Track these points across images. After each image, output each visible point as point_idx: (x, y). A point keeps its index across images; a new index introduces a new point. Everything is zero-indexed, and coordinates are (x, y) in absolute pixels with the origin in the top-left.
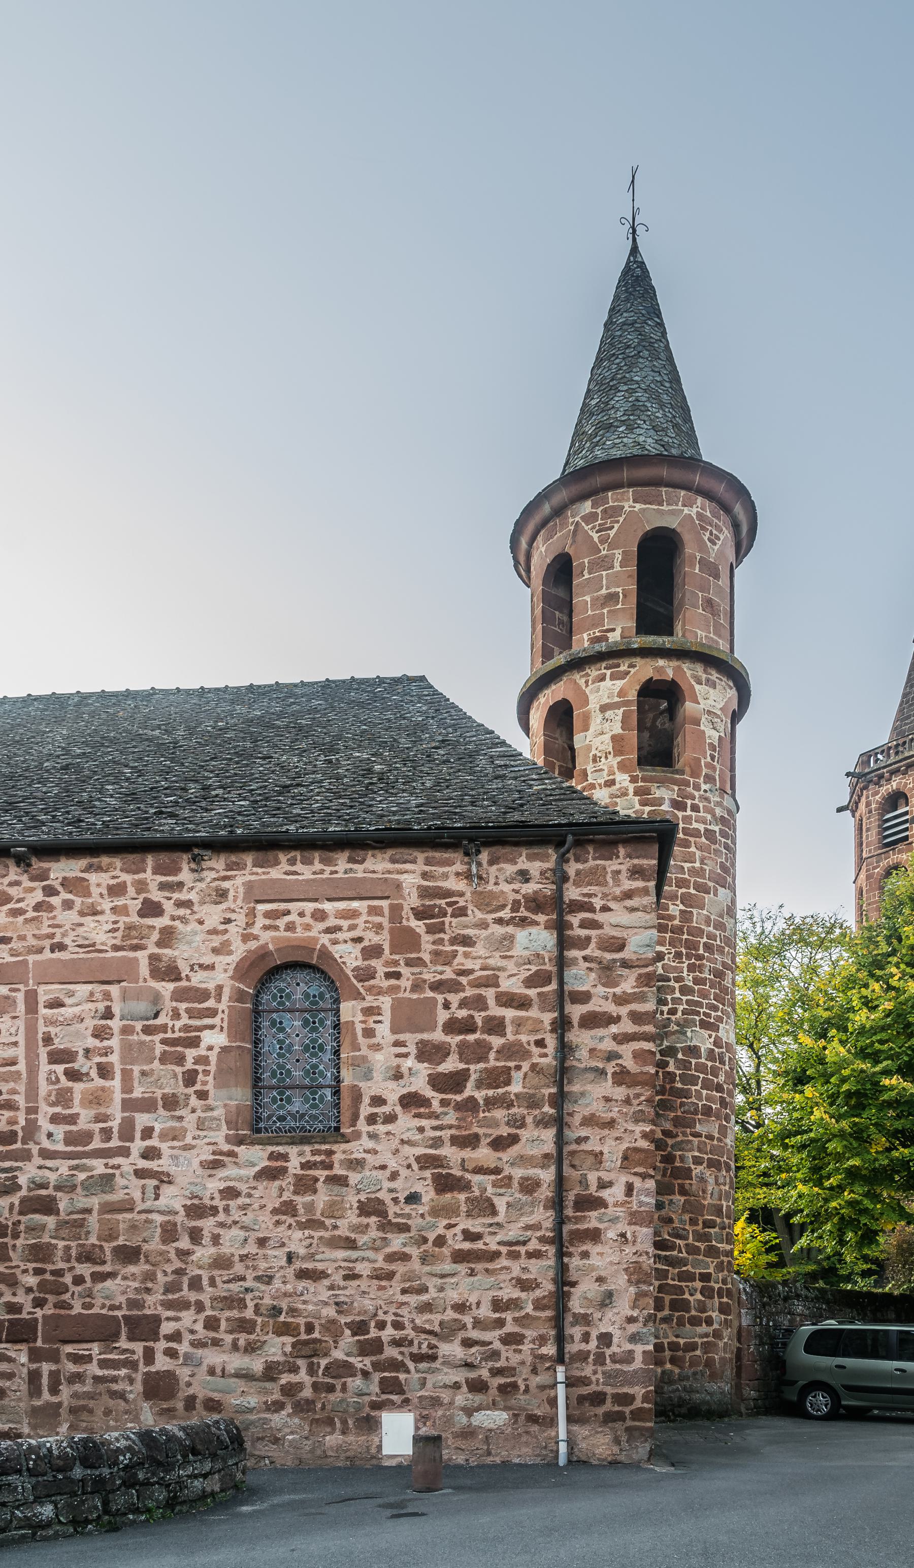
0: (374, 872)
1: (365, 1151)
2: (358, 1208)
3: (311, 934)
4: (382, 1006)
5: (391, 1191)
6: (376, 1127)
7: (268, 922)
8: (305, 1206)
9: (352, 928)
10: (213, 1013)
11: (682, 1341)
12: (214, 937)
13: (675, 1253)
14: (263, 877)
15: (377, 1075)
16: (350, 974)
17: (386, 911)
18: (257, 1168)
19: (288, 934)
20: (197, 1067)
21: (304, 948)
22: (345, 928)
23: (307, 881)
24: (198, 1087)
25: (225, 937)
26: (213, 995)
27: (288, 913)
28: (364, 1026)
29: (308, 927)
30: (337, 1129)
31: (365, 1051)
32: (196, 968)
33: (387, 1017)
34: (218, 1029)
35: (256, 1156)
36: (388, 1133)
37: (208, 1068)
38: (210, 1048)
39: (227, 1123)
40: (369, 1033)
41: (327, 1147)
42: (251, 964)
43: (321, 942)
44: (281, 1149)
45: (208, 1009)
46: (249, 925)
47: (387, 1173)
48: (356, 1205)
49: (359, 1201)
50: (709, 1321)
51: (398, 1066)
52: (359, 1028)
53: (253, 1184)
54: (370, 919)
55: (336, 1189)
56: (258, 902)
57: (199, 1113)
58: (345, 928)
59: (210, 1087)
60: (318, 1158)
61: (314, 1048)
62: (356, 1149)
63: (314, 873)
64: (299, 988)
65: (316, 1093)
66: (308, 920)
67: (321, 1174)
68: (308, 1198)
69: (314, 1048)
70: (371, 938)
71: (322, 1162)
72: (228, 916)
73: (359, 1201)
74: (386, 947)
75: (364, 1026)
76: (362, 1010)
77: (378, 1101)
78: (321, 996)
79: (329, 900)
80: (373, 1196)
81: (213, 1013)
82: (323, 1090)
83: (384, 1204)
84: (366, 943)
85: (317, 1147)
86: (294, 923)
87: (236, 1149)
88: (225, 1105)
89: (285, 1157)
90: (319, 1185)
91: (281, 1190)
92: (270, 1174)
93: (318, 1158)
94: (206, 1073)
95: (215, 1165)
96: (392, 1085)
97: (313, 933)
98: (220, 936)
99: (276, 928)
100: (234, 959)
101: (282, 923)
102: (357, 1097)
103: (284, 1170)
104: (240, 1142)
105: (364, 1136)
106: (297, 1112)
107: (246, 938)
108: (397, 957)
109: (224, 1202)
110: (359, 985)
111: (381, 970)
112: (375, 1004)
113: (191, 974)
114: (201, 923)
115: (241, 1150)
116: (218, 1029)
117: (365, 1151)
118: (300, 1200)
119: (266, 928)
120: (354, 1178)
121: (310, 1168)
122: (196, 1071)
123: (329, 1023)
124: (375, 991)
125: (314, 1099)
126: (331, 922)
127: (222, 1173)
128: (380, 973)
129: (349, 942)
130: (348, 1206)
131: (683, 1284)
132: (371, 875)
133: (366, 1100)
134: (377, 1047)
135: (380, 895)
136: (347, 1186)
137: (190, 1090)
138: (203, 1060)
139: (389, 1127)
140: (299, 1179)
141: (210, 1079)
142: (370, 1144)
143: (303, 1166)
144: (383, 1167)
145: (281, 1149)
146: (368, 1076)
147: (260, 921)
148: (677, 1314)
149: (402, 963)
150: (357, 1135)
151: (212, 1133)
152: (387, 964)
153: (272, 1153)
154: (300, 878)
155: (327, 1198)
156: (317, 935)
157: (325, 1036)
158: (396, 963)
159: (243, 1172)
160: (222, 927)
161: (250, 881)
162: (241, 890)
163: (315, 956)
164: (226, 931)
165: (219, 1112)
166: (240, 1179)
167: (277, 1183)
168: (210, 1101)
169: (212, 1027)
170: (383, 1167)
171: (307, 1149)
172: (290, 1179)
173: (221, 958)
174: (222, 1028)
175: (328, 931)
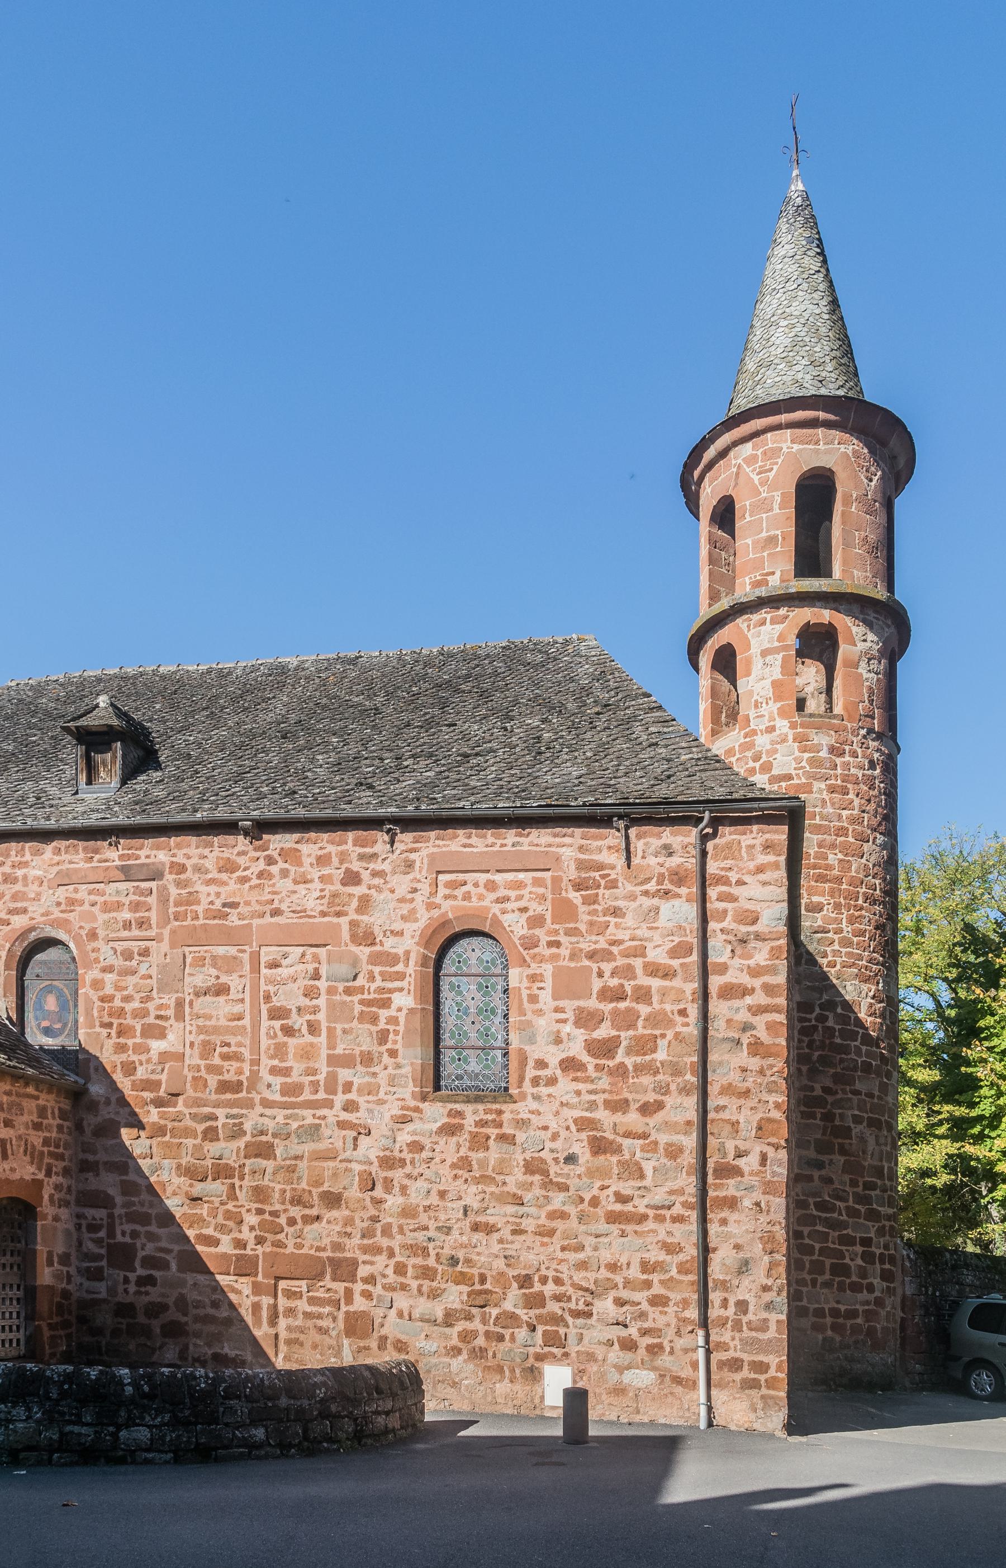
5: (552, 1151)
6: (539, 1089)
7: (448, 892)
9: (520, 898)
10: (401, 976)
11: (843, 1308)
12: (403, 905)
13: (835, 1215)
16: (517, 942)
17: (549, 882)
18: (439, 1124)
19: (465, 903)
21: (478, 916)
23: (481, 853)
27: (465, 883)
29: (481, 897)
31: (529, 1016)
33: (548, 984)
34: (405, 992)
35: (436, 1113)
36: (549, 1096)
40: (533, 999)
44: (458, 1107)
45: (397, 973)
47: (549, 1134)
48: (522, 1163)
50: (870, 1288)
51: (558, 1032)
52: (525, 993)
53: (435, 1138)
54: (534, 889)
55: (505, 1146)
56: (439, 872)
60: (490, 1117)
62: (523, 1109)
64: (471, 953)
66: (481, 890)
67: (492, 1132)
68: (481, 1155)
70: (536, 908)
74: (548, 917)
77: (541, 1064)
80: (536, 1155)
81: (401, 976)
84: (531, 913)
85: (489, 1106)
86: (469, 892)
87: (421, 1105)
88: (412, 1064)
89: (460, 1114)
90: (491, 1142)
91: (459, 1146)
92: (450, 1130)
95: (404, 1120)
96: (553, 1049)
97: (486, 903)
99: (455, 897)
100: (421, 924)
101: (459, 892)
103: (461, 1127)
104: (424, 1098)
105: (529, 1097)
107: (430, 906)
108: (557, 927)
109: (411, 1155)
110: (525, 953)
111: (544, 939)
112: (538, 972)
113: (384, 940)
114: (393, 891)
115: (425, 1106)
116: (405, 992)
119: (446, 897)
120: (520, 1137)
124: (538, 958)
126: (502, 892)
127: (410, 1127)
131: (844, 1248)
132: (534, 848)
133: (531, 1063)
134: (540, 1013)
139: (550, 1090)
140: (474, 1136)
141: (399, 1038)
142: (534, 1105)
144: (545, 1128)
145: (458, 1107)
146: (532, 1040)
147: (442, 891)
148: (837, 1279)
149: (561, 932)
150: (523, 1096)
151: (401, 1090)
154: (475, 850)
157: (497, 1000)
158: (556, 932)
160: (410, 896)
162: (425, 861)
165: (407, 1070)
167: (455, 1139)
168: (399, 1060)
169: (401, 990)
170: (545, 1128)
171: (481, 1107)
172: (466, 1136)
174: (18, 1327)
175: (498, 901)
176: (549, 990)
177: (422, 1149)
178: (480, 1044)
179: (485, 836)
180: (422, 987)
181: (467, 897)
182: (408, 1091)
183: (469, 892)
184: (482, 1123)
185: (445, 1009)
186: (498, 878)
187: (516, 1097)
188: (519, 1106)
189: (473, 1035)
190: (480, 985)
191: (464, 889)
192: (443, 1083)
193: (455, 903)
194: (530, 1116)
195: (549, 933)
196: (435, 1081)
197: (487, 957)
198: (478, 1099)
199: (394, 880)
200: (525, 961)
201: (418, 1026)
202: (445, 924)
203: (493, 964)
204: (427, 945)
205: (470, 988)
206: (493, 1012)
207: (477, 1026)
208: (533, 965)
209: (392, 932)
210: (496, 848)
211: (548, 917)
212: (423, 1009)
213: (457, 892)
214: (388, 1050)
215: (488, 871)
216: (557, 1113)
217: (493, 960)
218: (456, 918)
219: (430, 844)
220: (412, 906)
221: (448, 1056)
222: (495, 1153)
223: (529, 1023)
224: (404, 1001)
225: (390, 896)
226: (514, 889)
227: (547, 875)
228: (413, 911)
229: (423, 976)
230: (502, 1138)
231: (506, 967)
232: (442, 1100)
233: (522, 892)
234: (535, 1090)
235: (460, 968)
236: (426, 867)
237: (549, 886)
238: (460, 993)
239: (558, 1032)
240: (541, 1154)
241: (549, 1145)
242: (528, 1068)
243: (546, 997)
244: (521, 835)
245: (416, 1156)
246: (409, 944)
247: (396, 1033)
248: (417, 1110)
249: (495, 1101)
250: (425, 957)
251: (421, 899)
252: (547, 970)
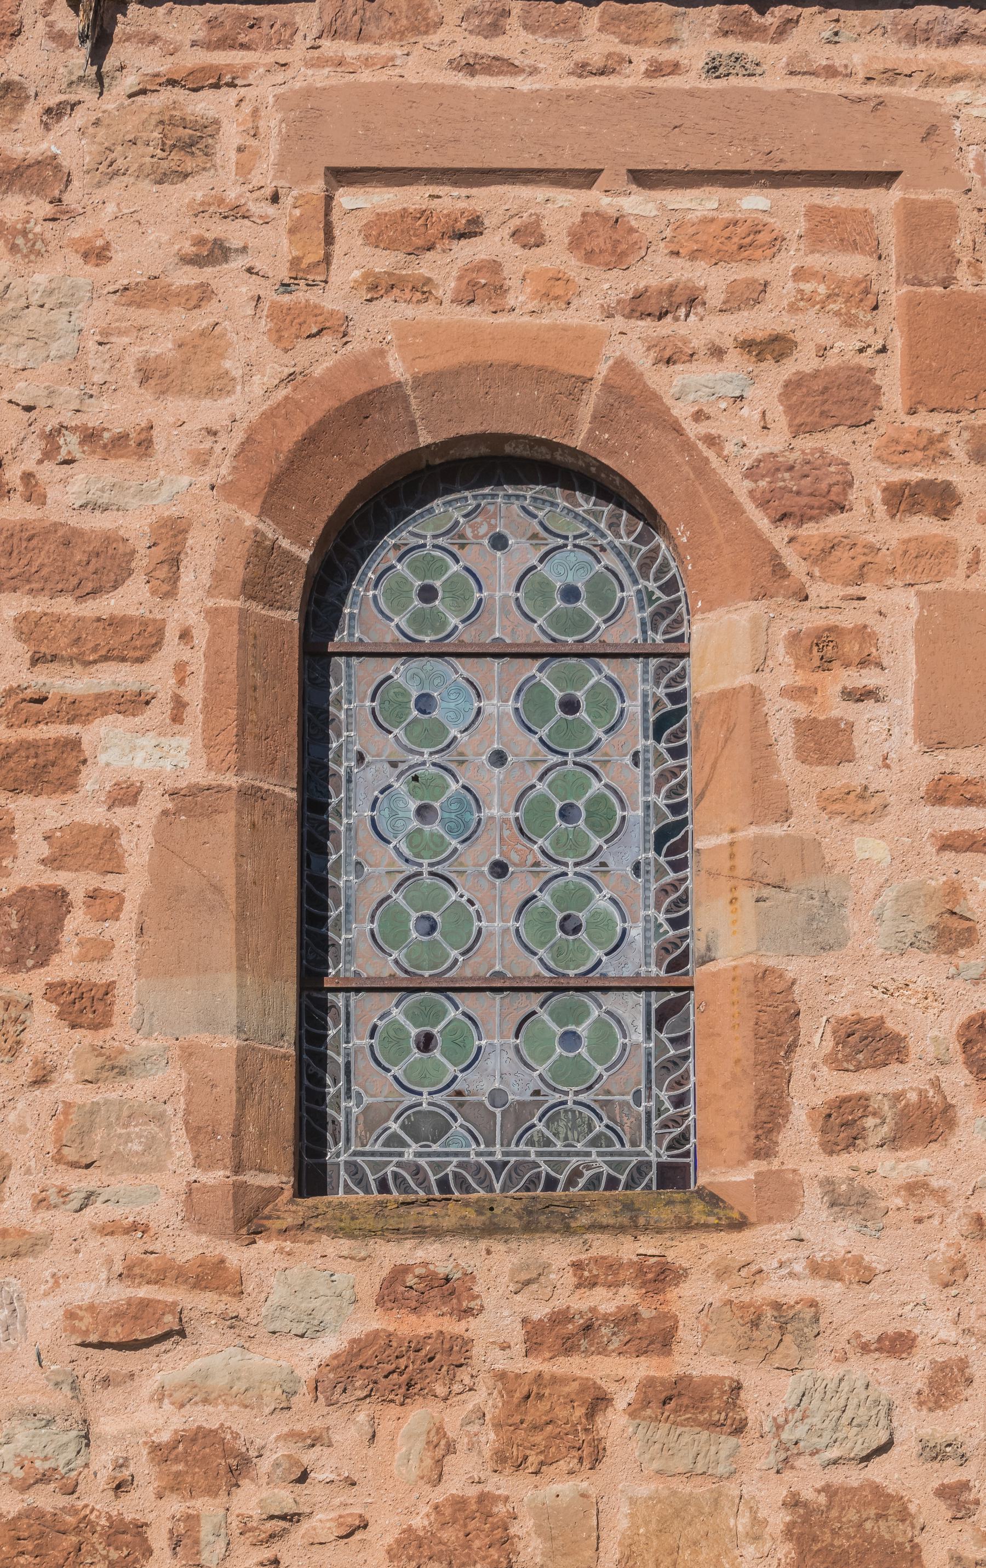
0: (831, 72)
1: (815, 1269)
2: (789, 1532)
3: (571, 318)
4: (881, 628)
5: (935, 1453)
6: (863, 1159)
7: (384, 262)
8: (552, 1523)
9: (752, 295)
10: (138, 642)
12: (151, 315)
14: (366, 76)
15: (869, 929)
16: (741, 488)
17: (890, 233)
18: (330, 1346)
19: (476, 315)
20: (61, 878)
21: (541, 374)
22: (715, 297)
23: (553, 99)
24: (65, 967)
25: (201, 320)
26: (141, 563)
27: (471, 229)
28: (802, 710)
29: (555, 291)
30: (673, 1176)
31: (807, 820)
32: (70, 444)
33: (901, 673)
34: (158, 712)
35: (323, 1289)
36: (916, 1189)
37: (111, 884)
38: (125, 795)
39: (195, 1133)
40: (825, 742)
41: (648, 1246)
42: (311, 439)
43: (614, 350)
44: (435, 1255)
45: (115, 623)
46: (308, 272)
47: (916, 1371)
48: (779, 1520)
49: (794, 1502)
51: (954, 890)
52: (782, 717)
53: (308, 1415)
54: (816, 261)
55: (691, 1442)
56: (342, 176)
57: (67, 1087)
58: (715, 297)
59: (119, 969)
60: (605, 1301)
61: (567, 813)
62: (781, 1257)
63: (582, 69)
64: (495, 558)
65: (580, 1015)
66: (556, 257)
67: (622, 1373)
68: (561, 1487)
69: (567, 813)
70: (827, 340)
71: (626, 1319)
72: (217, 229)
73: (794, 1502)
74: (891, 379)
75: (802, 710)
76: (795, 637)
77: (870, 1042)
78: (601, 592)
79: (643, 178)
80: (853, 1476)
81: (138, 642)
82: (610, 1001)
83: (904, 1516)
84: (803, 361)
85: (603, 1246)
86: (494, 267)
87: (236, 1256)
88: (188, 1053)
89: (448, 1291)
90: (615, 1424)
91: (441, 1447)
92: (390, 1372)
93: (605, 1301)
94: (104, 904)
95: (140, 1334)
96: (925, 970)
97: (582, 314)
98: (178, 315)
99: (423, 290)
100: (247, 401)
101: (446, 266)
102: (777, 1029)
103: (452, 1356)
104: (251, 1222)
105: (813, 1198)
106: (496, 1096)
107: (296, 326)
108: (936, 423)
109: (175, 1505)
110: (778, 536)
111: (872, 477)
112: (848, 618)
113: (48, 472)
114: (97, 254)
115: (257, 1259)
116: (158, 712)
117: (815, 1269)
118: (522, 1493)
119: (377, 287)
120: (768, 1393)
121: (568, 1347)
122: (60, 896)
123: (634, 707)
124: (844, 561)
125: (571, 1040)
126: (656, 271)
127: (168, 1367)
128: (868, 489)
129: (734, 357)
130: (742, 1523)
132: (819, 85)
133: (816, 1040)
134: (860, 805)
135: (858, 164)
136: (739, 1429)
137: (33, 983)
138: (100, 849)
139: (920, 1162)
140: (524, 1396)
141: (121, 931)
142: (838, 1238)
143: (536, 1337)
144: (898, 1345)
145: (435, 1255)
146: (821, 934)
147: (354, 260)
149: (958, 446)
150: (780, 1197)
151: (121, 1183)
152: (897, 450)
153: (399, 1272)
154: (523, 84)
155: (644, 1490)
156: (594, 321)
157: (625, 770)
158: (933, 447)
159: (266, 1360)
160: (187, 277)
161: (309, 93)
162: (272, 123)
163: (586, 412)
164: (204, 294)
165: (158, 1083)
166: (245, 1398)
167: (418, 1415)
168: (120, 1034)
169: (134, 703)
170: (898, 1345)
171: (557, 1254)
172: (485, 1397)
173: (177, 406)
174: (179, 706)
175: (641, 306)
176: (903, 704)
177: (238, 1468)
178: (531, 968)
179: (569, 28)
180: (247, 696)
181: (483, 287)
182: (163, 1186)
183: (494, 267)
184: (562, 1334)
185: (351, 814)
186: (638, 205)
187: (739, 1205)
188: (764, 1241)
189: (498, 925)
190: (531, 695)
191: (466, 252)
192: (338, 1155)
193: (423, 313)
194: (813, 1288)
195: (897, 450)
196: (305, 1147)
197: (566, 570)
198: (533, 1222)
199: (101, 209)
200: (779, 570)
201: (224, 869)
202: (371, 405)
203: (601, 600)
204: (276, 496)
205: (489, 711)
206: (602, 816)
207: (520, 884)
208: (820, 591)
209: (90, 437)
210: (630, 79)
211: (891, 379)
212: (249, 794)
213: (427, 266)
214: (55, 991)
215: (587, 178)
216: (955, 1273)
217: (596, 584)
218: (433, 383)
219: (297, 53)
220: (201, 320)
221: (358, 1029)
222: (634, 1470)
223: (807, 853)
224: (157, 751)
225: (85, 274)
226: (720, 258)
227: (882, 202)
228: (208, 342)
229: (252, 641)
230: (674, 1400)
231: (667, 613)
232: (347, 1227)
233: (760, 272)
234: (839, 1166)
235: (436, 622)
236: (272, 148)
237: (892, 251)
238: (431, 733)
239: (954, 890)
240: (877, 1471)
241: (914, 1426)
242: (801, 1064)
243: (888, 736)
244: (750, 32)
245: (208, 1509)
246: (187, 500)
247: (104, 904)
248: (211, 1276)
249: (632, 1223)
250: (263, 555)
251: (247, 288)
252: (895, 613)
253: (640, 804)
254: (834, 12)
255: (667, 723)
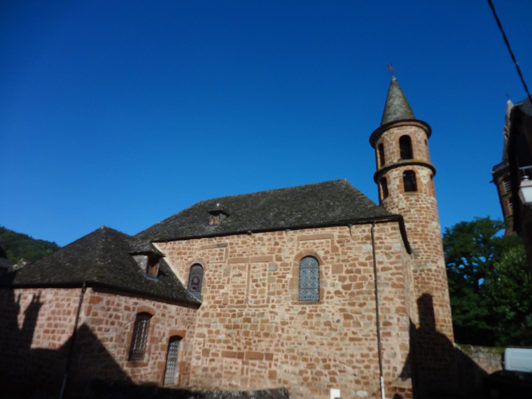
9: (322, 246)
10: (289, 269)
15: (329, 285)
27: (307, 243)
29: (311, 247)
59: (288, 289)
62: (323, 306)
66: (312, 245)
67: (314, 313)
70: (327, 249)
77: (329, 293)
90: (314, 317)
91: (304, 318)
92: (302, 313)
93: (314, 309)
95: (288, 310)
97: (313, 248)
101: (305, 246)
119: (302, 247)
126: (317, 245)
134: (328, 278)
141: (288, 287)
147: (301, 246)
171: (311, 306)
198: (311, 304)
206: (315, 278)
248: (292, 307)
249: (315, 304)
252: (330, 266)
253: (317, 277)
254: (406, 230)
255: (319, 272)
